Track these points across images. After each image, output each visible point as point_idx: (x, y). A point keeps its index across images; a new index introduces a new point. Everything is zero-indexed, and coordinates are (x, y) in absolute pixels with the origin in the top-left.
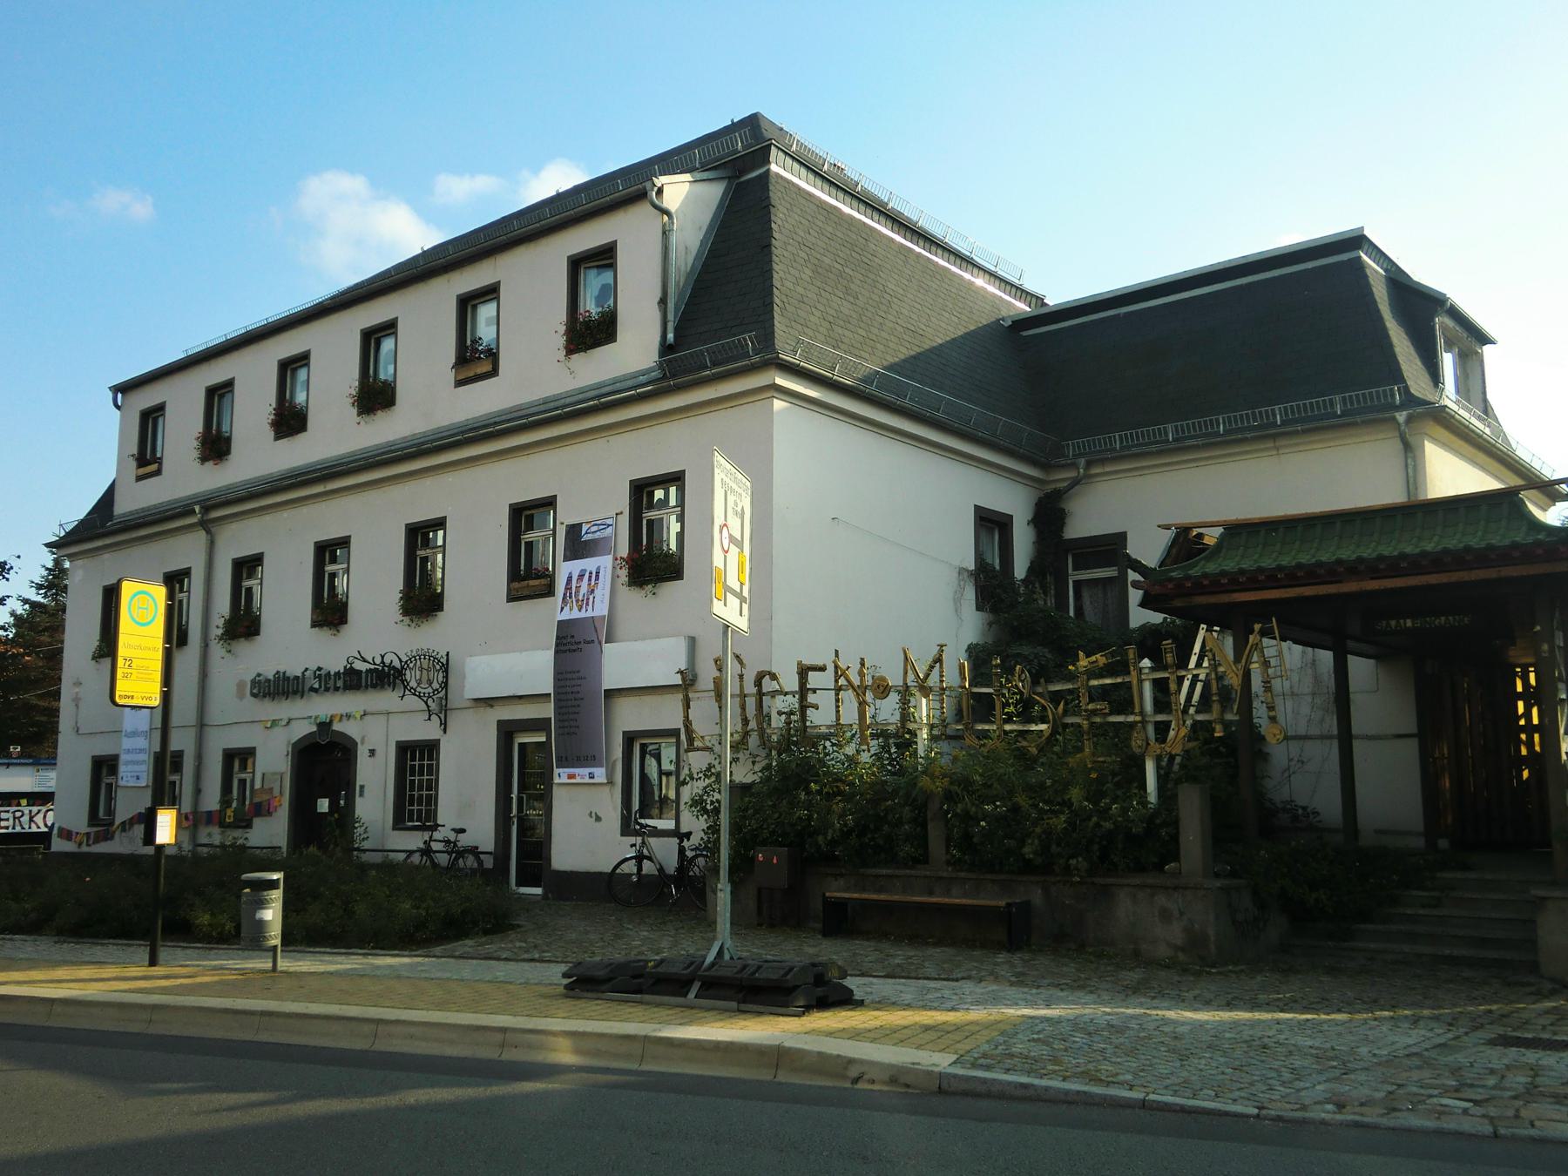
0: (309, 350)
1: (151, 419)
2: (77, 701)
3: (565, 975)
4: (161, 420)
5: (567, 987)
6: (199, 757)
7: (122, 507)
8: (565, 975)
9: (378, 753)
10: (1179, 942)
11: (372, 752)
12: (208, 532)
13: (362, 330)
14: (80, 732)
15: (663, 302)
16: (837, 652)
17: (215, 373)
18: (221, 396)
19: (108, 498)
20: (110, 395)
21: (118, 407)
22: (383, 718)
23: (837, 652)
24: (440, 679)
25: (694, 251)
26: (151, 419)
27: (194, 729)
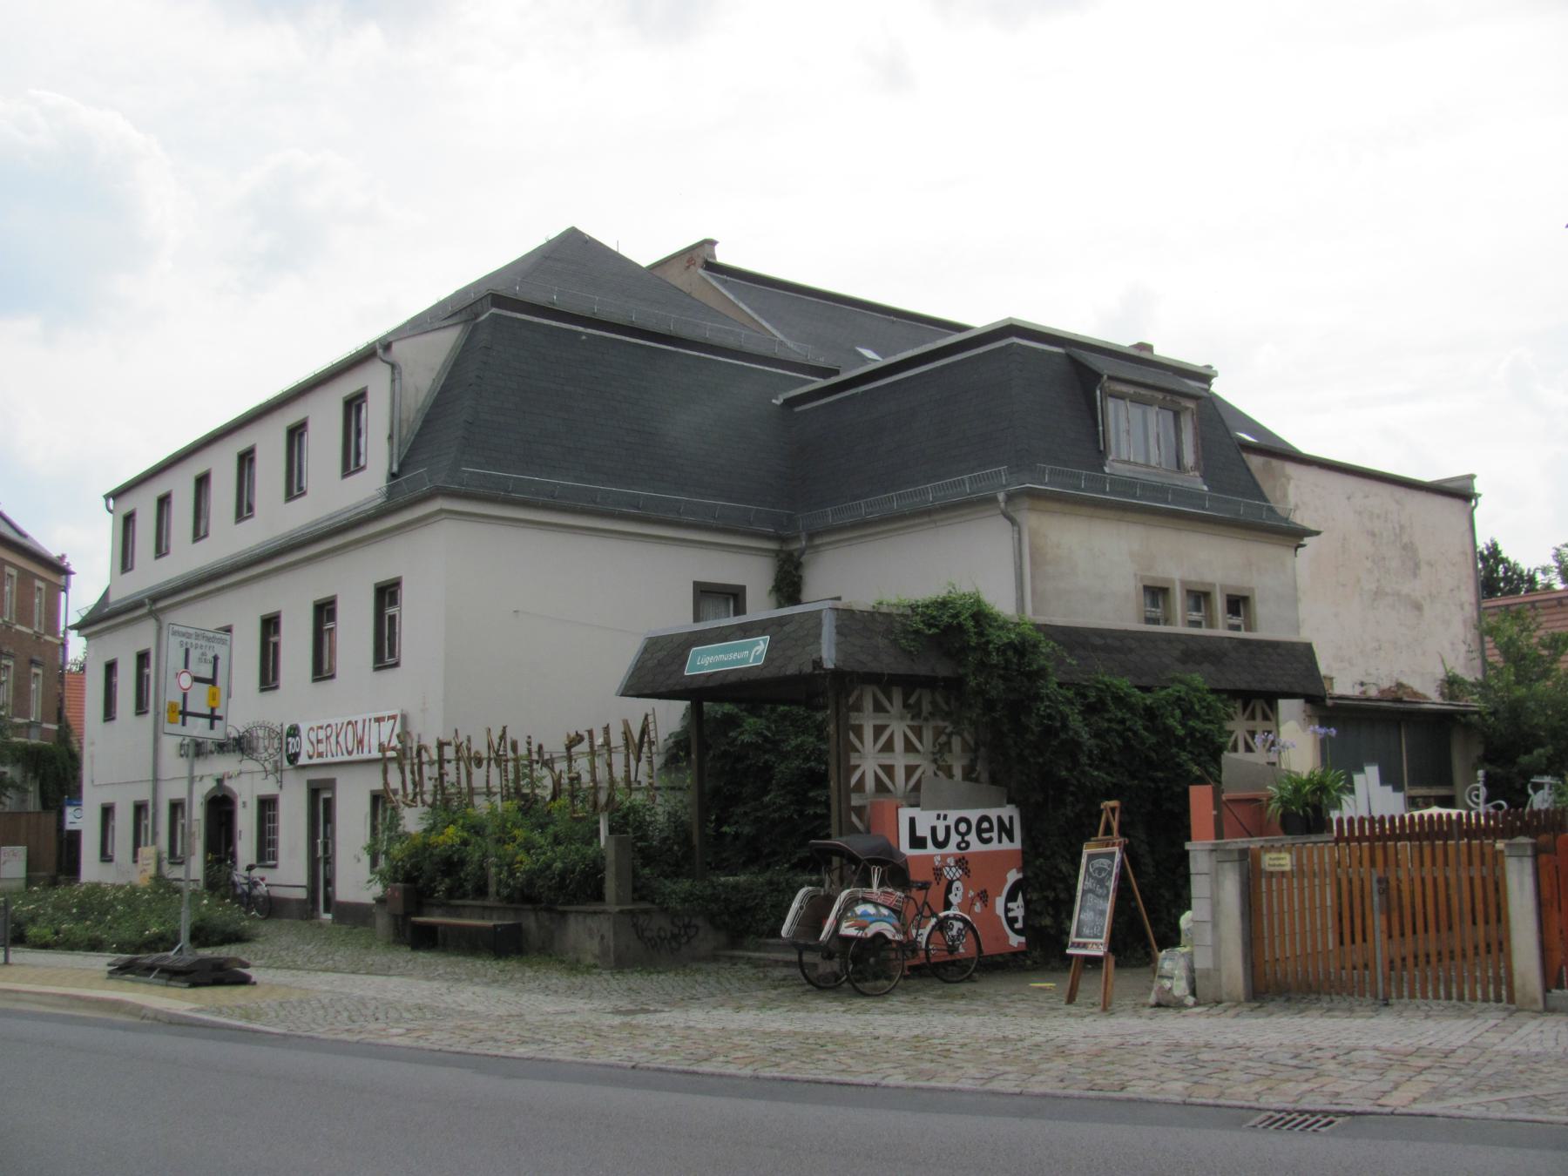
0: (171, 491)
1: (129, 520)
2: (92, 757)
3: (109, 965)
4: (364, 405)
5: (110, 972)
6: (155, 804)
7: (113, 598)
8: (109, 965)
9: (248, 804)
10: (597, 952)
11: (244, 803)
12: (157, 620)
13: (344, 398)
14: (96, 783)
15: (391, 437)
16: (456, 731)
17: (291, 416)
18: (301, 435)
19: (106, 595)
20: (104, 500)
21: (110, 511)
22: (250, 775)
23: (456, 731)
24: (276, 745)
25: (421, 398)
26: (129, 520)
27: (151, 783)
